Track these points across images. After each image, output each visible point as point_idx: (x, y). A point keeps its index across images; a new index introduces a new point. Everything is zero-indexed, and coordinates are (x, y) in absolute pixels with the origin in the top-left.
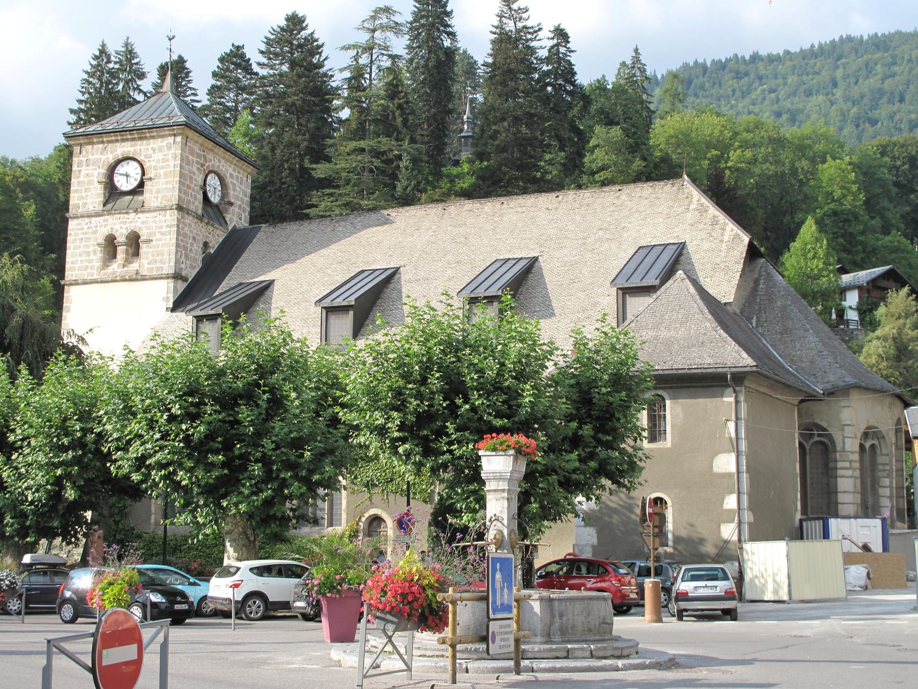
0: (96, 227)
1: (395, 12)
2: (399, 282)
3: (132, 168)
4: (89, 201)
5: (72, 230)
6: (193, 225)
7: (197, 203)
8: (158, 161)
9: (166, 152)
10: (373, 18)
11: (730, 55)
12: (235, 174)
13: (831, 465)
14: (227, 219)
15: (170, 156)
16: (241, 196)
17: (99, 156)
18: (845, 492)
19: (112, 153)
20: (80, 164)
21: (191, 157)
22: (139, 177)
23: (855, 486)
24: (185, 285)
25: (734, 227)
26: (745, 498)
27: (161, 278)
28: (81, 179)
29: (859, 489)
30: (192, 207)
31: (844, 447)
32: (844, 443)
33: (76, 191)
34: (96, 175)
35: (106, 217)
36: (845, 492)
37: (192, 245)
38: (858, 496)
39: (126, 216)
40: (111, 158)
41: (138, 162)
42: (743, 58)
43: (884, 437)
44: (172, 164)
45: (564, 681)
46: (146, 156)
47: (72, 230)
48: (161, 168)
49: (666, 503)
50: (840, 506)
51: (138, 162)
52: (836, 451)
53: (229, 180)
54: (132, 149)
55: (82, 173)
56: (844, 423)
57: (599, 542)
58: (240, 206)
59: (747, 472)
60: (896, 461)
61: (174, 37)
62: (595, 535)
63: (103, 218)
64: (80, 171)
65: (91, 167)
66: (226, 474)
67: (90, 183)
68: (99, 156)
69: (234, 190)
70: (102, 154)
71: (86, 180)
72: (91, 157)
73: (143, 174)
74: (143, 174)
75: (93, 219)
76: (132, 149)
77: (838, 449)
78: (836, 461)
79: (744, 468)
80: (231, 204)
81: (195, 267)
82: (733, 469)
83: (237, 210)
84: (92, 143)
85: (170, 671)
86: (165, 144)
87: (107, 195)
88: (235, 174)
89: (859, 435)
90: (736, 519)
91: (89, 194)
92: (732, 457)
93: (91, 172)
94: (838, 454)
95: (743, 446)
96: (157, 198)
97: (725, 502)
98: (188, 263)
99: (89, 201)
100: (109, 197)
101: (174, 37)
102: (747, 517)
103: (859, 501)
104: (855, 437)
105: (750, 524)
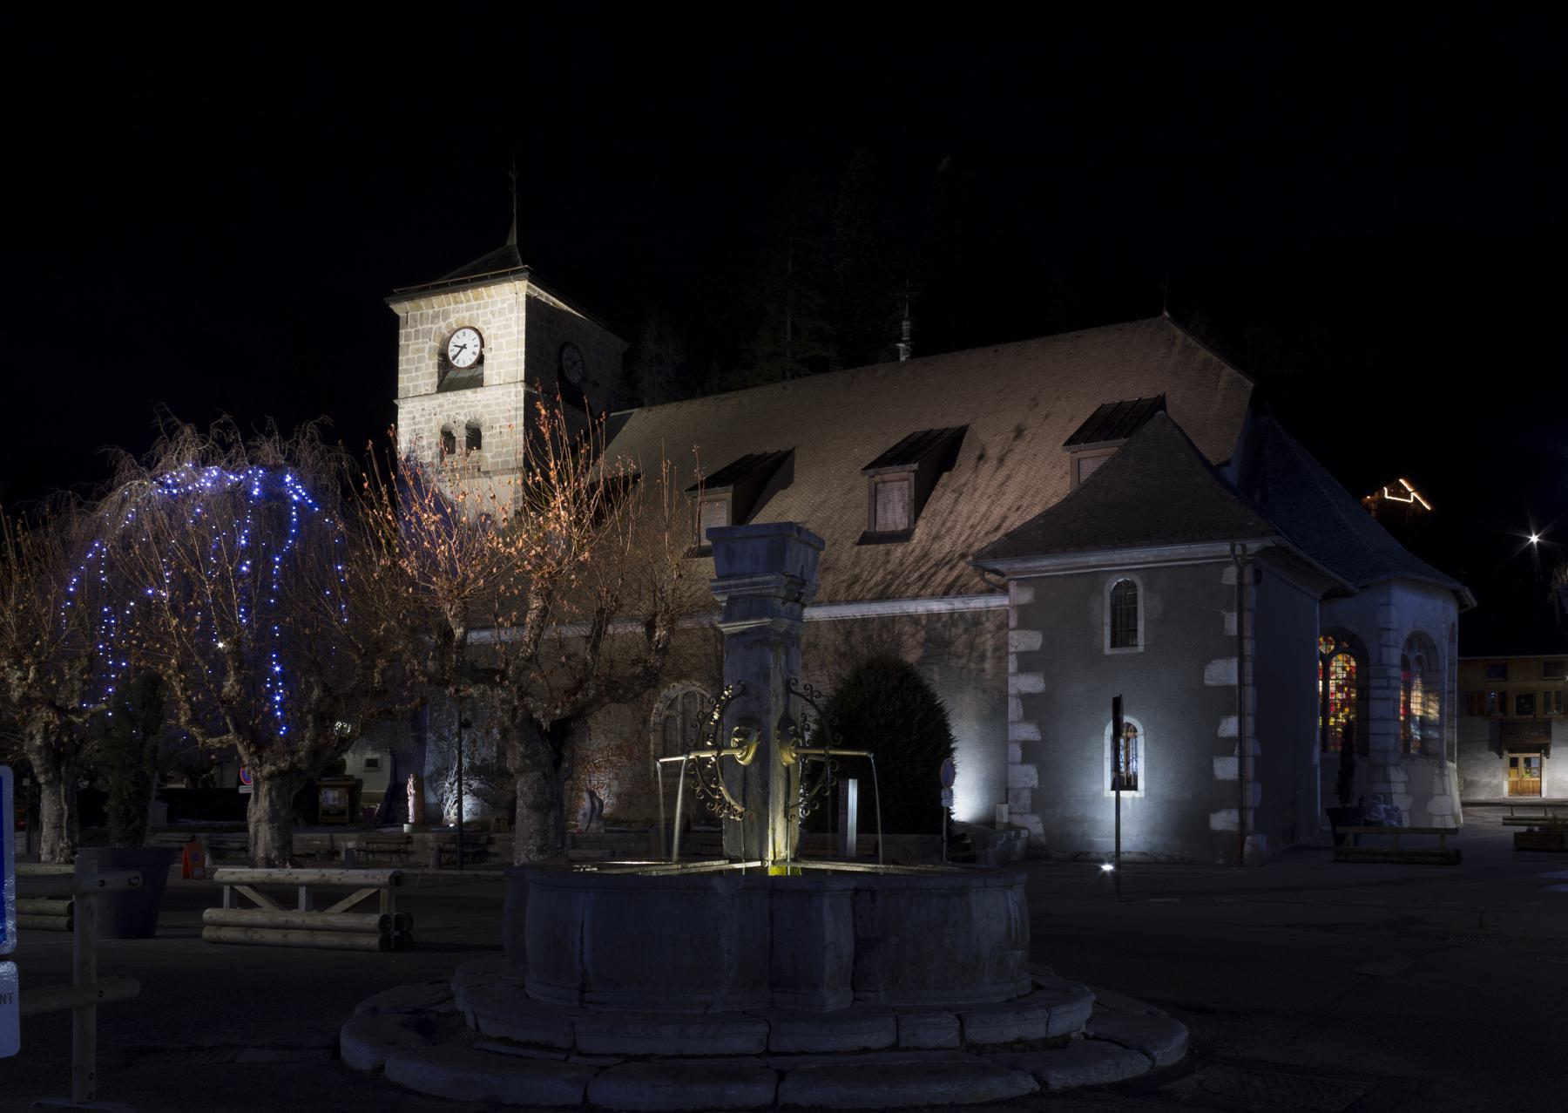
0: (430, 414)
2: (792, 463)
4: (421, 382)
5: (403, 419)
8: (499, 328)
9: (507, 316)
15: (513, 321)
17: (430, 326)
19: (444, 320)
20: (408, 337)
22: (477, 350)
25: (1233, 372)
26: (1250, 720)
28: (410, 356)
33: (407, 371)
41: (476, 331)
43: (1434, 647)
44: (515, 330)
45: (1179, 566)
46: (485, 323)
47: (403, 419)
48: (503, 336)
49: (1135, 731)
51: (476, 331)
55: (411, 348)
59: (1254, 684)
60: (1449, 680)
64: (408, 345)
65: (420, 340)
66: (343, 442)
67: (420, 360)
68: (430, 326)
70: (432, 323)
71: (416, 356)
73: (482, 345)
74: (482, 345)
79: (1249, 679)
82: (1234, 681)
90: (1236, 751)
91: (419, 374)
92: (1234, 663)
93: (421, 345)
95: (1249, 648)
96: (499, 374)
97: (1221, 728)
99: (421, 382)
102: (1252, 748)
105: (1256, 758)
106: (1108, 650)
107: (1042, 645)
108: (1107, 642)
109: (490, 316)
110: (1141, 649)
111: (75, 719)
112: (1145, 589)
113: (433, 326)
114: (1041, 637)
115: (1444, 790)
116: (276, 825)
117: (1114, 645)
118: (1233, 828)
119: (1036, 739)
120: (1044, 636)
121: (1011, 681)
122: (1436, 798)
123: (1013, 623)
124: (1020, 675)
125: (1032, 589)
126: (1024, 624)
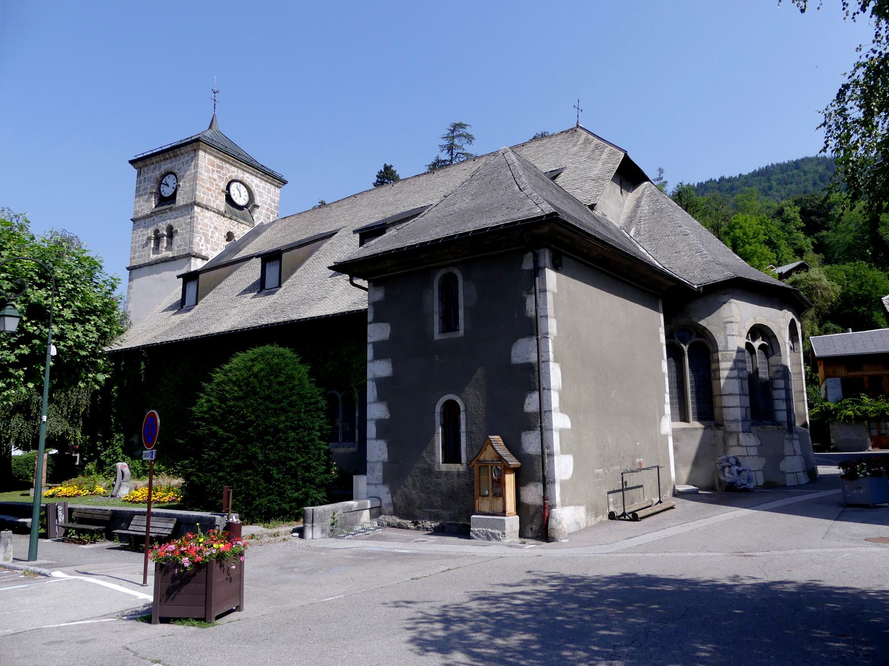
1: (465, 125)
3: (170, 180)
6: (214, 218)
7: (218, 202)
10: (453, 131)
11: (708, 179)
12: (261, 185)
13: (713, 366)
14: (254, 218)
16: (269, 201)
18: (730, 394)
21: (210, 167)
23: (742, 388)
24: (206, 262)
27: (184, 257)
28: (141, 193)
29: (747, 391)
30: (213, 205)
31: (727, 346)
32: (726, 342)
34: (149, 188)
35: (154, 217)
36: (730, 394)
37: (212, 232)
38: (747, 399)
39: (165, 214)
40: (157, 173)
42: (715, 180)
50: (725, 411)
52: (717, 351)
53: (254, 188)
54: (170, 166)
56: (725, 320)
57: (389, 458)
58: (268, 209)
61: (218, 92)
62: (386, 450)
63: (152, 218)
64: (140, 187)
68: (151, 174)
69: (261, 197)
70: (153, 172)
72: (146, 176)
75: (147, 220)
76: (170, 166)
77: (720, 348)
78: (718, 361)
80: (258, 207)
81: (217, 250)
83: (264, 211)
84: (146, 165)
85: (148, 570)
86: (189, 158)
87: (157, 202)
88: (261, 185)
89: (745, 334)
93: (146, 186)
94: (720, 354)
98: (209, 246)
100: (159, 204)
101: (218, 92)
103: (748, 404)
104: (740, 335)
106: (437, 336)
107: (390, 335)
108: (436, 328)
109: (181, 165)
110: (461, 332)
111: (227, 395)
112: (464, 280)
113: (153, 174)
114: (389, 327)
115: (428, 651)
116: (149, 454)
117: (443, 331)
118: (781, 420)
119: (387, 417)
120: (391, 326)
121: (370, 366)
122: (761, 468)
123: (370, 317)
124: (375, 361)
125: (383, 288)
126: (754, 339)
